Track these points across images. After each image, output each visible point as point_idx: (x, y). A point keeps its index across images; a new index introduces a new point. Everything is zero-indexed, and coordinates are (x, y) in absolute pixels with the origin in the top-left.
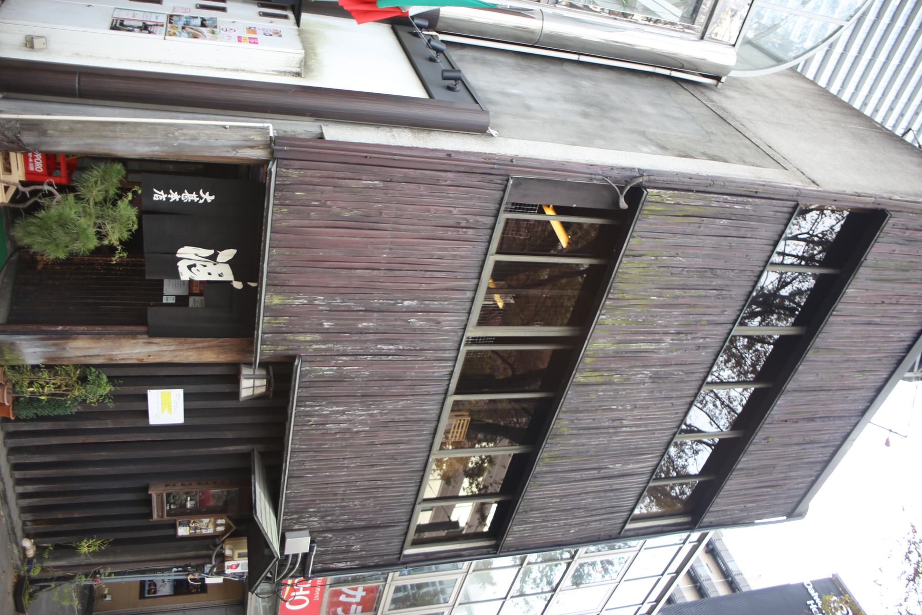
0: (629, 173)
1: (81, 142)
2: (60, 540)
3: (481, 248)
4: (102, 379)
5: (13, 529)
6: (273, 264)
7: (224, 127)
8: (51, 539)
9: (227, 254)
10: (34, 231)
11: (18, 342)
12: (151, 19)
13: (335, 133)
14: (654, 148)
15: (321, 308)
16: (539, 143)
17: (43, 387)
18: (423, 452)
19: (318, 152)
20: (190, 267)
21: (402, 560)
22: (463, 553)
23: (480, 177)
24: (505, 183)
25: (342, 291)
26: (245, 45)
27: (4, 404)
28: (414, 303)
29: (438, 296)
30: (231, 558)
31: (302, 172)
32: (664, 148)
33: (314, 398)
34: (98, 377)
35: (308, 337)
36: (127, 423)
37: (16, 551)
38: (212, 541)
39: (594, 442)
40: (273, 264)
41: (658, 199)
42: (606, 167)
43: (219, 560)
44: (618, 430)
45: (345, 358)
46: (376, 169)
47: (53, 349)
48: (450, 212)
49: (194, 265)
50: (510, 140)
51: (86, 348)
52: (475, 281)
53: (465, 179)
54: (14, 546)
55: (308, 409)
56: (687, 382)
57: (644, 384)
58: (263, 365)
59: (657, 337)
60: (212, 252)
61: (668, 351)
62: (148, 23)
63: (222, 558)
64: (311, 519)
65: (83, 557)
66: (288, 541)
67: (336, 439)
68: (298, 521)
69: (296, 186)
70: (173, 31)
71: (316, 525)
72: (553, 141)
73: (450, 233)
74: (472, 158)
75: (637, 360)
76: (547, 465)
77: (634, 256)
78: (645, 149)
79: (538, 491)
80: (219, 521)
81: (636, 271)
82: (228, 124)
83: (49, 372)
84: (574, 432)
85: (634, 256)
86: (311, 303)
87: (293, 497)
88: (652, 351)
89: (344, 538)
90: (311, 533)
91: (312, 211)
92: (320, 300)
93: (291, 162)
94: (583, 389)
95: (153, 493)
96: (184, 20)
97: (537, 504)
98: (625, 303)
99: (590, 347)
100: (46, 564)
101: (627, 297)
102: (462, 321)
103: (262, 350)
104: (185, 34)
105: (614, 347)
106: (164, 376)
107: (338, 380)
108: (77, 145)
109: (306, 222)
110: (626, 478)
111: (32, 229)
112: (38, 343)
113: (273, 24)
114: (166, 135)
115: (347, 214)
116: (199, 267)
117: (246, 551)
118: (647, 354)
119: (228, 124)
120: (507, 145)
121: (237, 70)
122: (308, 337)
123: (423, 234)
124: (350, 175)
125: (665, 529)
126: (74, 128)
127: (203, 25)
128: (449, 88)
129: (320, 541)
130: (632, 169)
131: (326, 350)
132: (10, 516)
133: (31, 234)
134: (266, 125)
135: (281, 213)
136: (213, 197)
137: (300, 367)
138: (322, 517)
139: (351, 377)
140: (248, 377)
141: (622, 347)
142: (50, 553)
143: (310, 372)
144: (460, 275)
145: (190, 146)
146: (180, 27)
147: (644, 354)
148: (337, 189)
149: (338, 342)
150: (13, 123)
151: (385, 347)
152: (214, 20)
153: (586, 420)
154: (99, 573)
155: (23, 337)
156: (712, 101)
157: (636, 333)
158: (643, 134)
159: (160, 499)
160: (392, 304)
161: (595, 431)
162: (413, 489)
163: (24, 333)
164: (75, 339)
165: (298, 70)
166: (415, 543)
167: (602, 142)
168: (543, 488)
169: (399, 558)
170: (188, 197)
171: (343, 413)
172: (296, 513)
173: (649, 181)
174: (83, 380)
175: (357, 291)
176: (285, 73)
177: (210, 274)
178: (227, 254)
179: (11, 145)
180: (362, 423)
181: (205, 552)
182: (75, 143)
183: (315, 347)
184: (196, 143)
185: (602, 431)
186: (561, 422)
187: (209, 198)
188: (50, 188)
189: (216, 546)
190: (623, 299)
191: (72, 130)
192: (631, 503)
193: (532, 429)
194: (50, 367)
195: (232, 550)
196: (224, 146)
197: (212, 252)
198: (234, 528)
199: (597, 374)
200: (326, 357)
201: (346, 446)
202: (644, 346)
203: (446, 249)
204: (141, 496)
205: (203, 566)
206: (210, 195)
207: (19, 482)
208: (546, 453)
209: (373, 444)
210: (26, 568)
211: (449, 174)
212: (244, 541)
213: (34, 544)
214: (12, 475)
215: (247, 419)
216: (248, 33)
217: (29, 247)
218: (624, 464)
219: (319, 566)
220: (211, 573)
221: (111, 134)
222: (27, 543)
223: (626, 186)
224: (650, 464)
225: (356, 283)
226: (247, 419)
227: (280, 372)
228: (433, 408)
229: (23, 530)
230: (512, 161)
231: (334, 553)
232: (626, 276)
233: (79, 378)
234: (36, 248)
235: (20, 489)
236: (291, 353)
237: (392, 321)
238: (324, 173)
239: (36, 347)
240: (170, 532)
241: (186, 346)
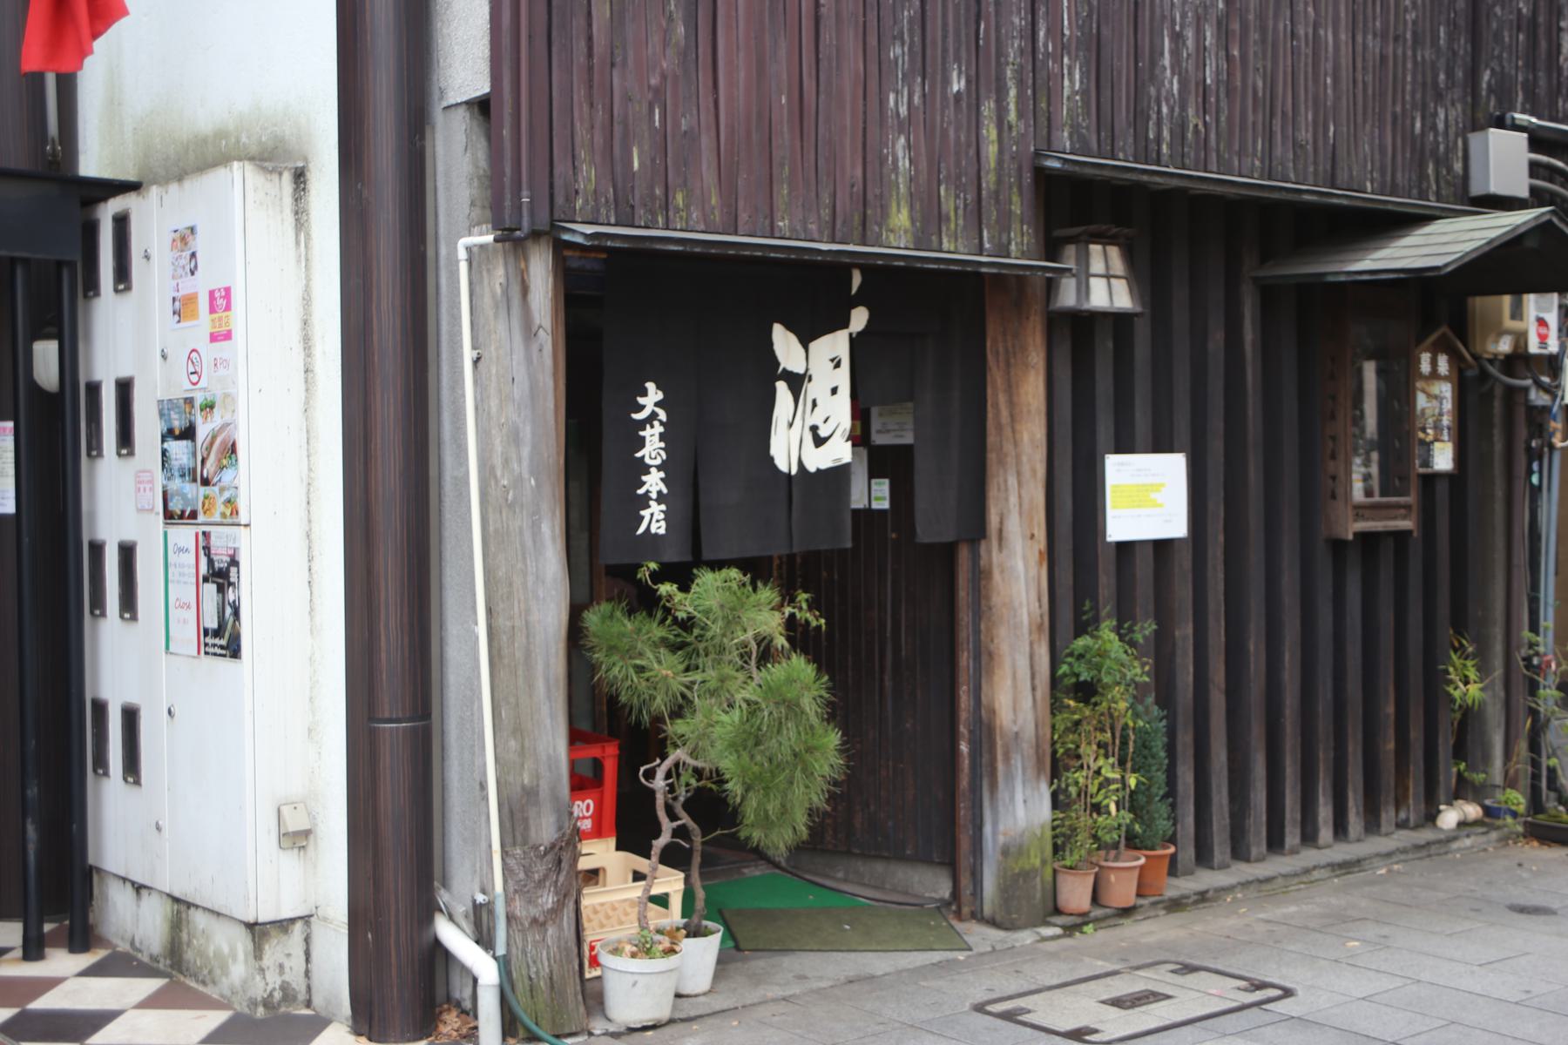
1: (545, 710)
4: (1087, 648)
5: (1418, 847)
6: (813, 227)
7: (476, 362)
8: (1442, 766)
9: (786, 348)
10: (778, 802)
11: (1001, 839)
12: (187, 564)
15: (917, 99)
17: (1108, 781)
20: (819, 441)
26: (237, 319)
27: (1142, 868)
30: (1521, 338)
33: (1139, 116)
34: (1081, 657)
35: (990, 132)
36: (1183, 592)
37: (1468, 842)
38: (1473, 388)
40: (813, 227)
45: (1042, 34)
49: (814, 429)
51: (1015, 686)
54: (1455, 845)
55: (1166, 134)
58: (1052, 250)
60: (781, 386)
62: (203, 569)
63: (1519, 360)
64: (1441, 126)
66: (1496, 187)
67: (1244, 56)
68: (1443, 162)
69: (618, 169)
70: (220, 507)
71: (1456, 112)
80: (1425, 367)
82: (468, 355)
83: (1067, 769)
86: (904, 126)
87: (1383, 174)
89: (1498, 37)
90: (1477, 126)
91: (677, 124)
92: (898, 103)
93: (558, 183)
96: (176, 484)
100: (1498, 779)
103: (1018, 249)
104: (227, 476)
106: (1076, 500)
107: (1095, 51)
108: (553, 717)
109: (706, 141)
111: (773, 807)
113: (154, 254)
114: (511, 506)
115: (681, 30)
116: (816, 418)
117: (1507, 300)
119: (468, 355)
121: (307, 341)
122: (990, 132)
126: (511, 726)
127: (188, 433)
129: (1500, 102)
131: (1021, 84)
132: (1389, 855)
133: (784, 810)
134: (462, 254)
135: (687, 206)
136: (650, 386)
137: (1064, 154)
138: (1439, 97)
139: (1090, 16)
140: (1084, 290)
142: (1472, 768)
143: (1075, 129)
145: (534, 447)
146: (203, 490)
148: (618, 60)
149: (1000, 53)
150: (511, 862)
152: (165, 408)
154: (1528, 659)
155: (988, 829)
159: (1367, 513)
163: (979, 828)
164: (993, 712)
165: (287, 177)
170: (653, 448)
171: (1177, 38)
172: (1422, 166)
174: (1086, 691)
177: (834, 391)
178: (786, 348)
179: (565, 865)
181: (1497, 405)
182: (548, 721)
183: (1012, 116)
184: (527, 432)
187: (652, 396)
188: (660, 774)
189: (1484, 376)
191: (518, 731)
194: (1056, 769)
195: (1501, 333)
196: (529, 360)
197: (781, 386)
198: (1444, 329)
200: (1040, 86)
201: (1263, 30)
206: (645, 393)
207: (1309, 837)
210: (1509, 820)
213: (1450, 804)
214: (1294, 852)
215: (1180, 296)
216: (194, 315)
217: (811, 812)
221: (520, 640)
222: (1449, 818)
226: (1180, 296)
227: (1074, 206)
229: (1417, 827)
231: (1532, 66)
233: (1086, 701)
234: (819, 800)
235: (1325, 834)
236: (1028, 178)
238: (579, 94)
239: (1012, 799)
240: (1442, 490)
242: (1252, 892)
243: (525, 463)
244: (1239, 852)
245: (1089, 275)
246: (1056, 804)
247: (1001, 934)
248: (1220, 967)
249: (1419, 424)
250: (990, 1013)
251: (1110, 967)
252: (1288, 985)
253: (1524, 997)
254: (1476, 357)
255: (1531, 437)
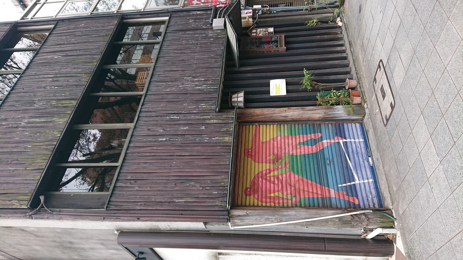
0: (38, 216)
2: (325, 25)
3: (125, 170)
13: (199, 225)
14: (28, 229)
16: (91, 228)
18: (158, 66)
19: (207, 215)
21: (169, 14)
22: (139, 16)
23: (123, 208)
24: (109, 206)
25: (195, 145)
28: (160, 140)
29: (148, 143)
30: (249, 17)
31: (214, 204)
32: (22, 230)
33: (210, 93)
35: (212, 121)
37: (345, 20)
38: (258, 25)
39: (68, 70)
41: (22, 203)
42: (51, 219)
43: (255, 16)
44: (54, 76)
46: (177, 208)
47: (330, 113)
48: (139, 188)
50: (107, 228)
52: (128, 152)
53: (130, 206)
56: (14, 101)
57: (39, 100)
58: (233, 108)
59: (29, 125)
61: (24, 118)
63: (253, 17)
65: (316, 18)
66: (222, 24)
68: (218, 34)
69: (217, 196)
71: (210, 32)
72: (84, 230)
73: (139, 176)
74: (126, 218)
75: (42, 112)
76: (95, 58)
77: (39, 169)
78: (33, 229)
79: (101, 45)
80: (255, 34)
81: (38, 161)
84: (79, 75)
85: (39, 169)
88: (32, 117)
92: (206, 139)
93: (219, 209)
94: (73, 97)
95: (284, 48)
97: (101, 39)
98: (46, 143)
99: (67, 119)
101: (44, 147)
102: (136, 131)
103: (232, 115)
105: (54, 119)
106: (279, 102)
107: (198, 101)
109: (212, 178)
110: (52, 51)
112: (337, 115)
115: (192, 183)
117: (242, 20)
118: (36, 116)
120: (109, 226)
121: (250, 254)
122: (212, 121)
123: (154, 175)
124: (190, 204)
125: (33, 24)
128: (142, 253)
130: (36, 218)
131: (204, 116)
134: (233, 228)
135: (224, 182)
138: (207, 36)
141: (49, 120)
143: (211, 105)
144: (137, 154)
147: (38, 116)
148: (197, 196)
149: (198, 119)
151: (175, 117)
153: (72, 81)
156: (2, 255)
157: (41, 127)
158: (37, 236)
160: (171, 138)
161: (68, 75)
162: (163, 48)
165: (219, 256)
166: (163, 22)
167: (58, 231)
168: (97, 47)
169: (171, 15)
172: (219, 38)
173: (25, 213)
175: (188, 145)
176: (226, 254)
180: (187, 81)
181: (262, 20)
183: (209, 117)
184: (266, 217)
185: (63, 75)
186: (85, 80)
189: (256, 23)
190: (47, 145)
192: (51, 38)
193: (99, 79)
198: (248, 31)
199: (65, 105)
200: (204, 112)
202: (37, 120)
203: (144, 168)
204: (290, 46)
205: (262, 14)
208: (95, 64)
209: (182, 71)
211: (139, 208)
212: (243, 25)
218: (53, 58)
219: (209, 12)
220: (259, 10)
222: (340, 24)
223: (40, 209)
224: (39, 58)
225: (189, 148)
227: (225, 105)
228: (153, 88)
230: (104, 219)
232: (44, 158)
235: (343, 48)
236: (220, 114)
237: (172, 130)
240: (277, 29)
241: (269, 116)
242: (356, 64)
243: (272, 217)
244: (347, 66)
245: (238, 101)
246: (339, 105)
247: (366, 115)
248: (375, 74)
249: (265, 35)
250: (387, 123)
251: (374, 95)
252: (379, 60)
253: (381, 13)
254: (253, 25)
255: (267, 13)
